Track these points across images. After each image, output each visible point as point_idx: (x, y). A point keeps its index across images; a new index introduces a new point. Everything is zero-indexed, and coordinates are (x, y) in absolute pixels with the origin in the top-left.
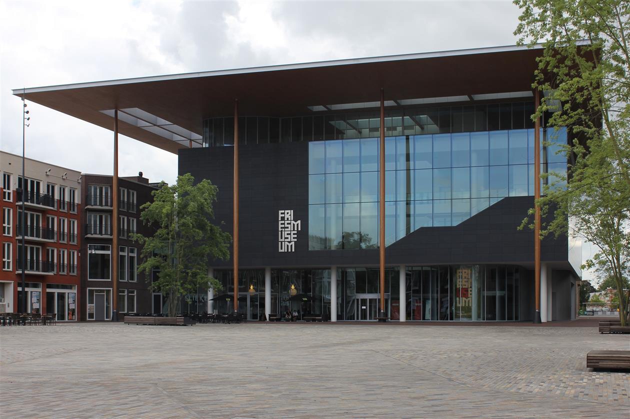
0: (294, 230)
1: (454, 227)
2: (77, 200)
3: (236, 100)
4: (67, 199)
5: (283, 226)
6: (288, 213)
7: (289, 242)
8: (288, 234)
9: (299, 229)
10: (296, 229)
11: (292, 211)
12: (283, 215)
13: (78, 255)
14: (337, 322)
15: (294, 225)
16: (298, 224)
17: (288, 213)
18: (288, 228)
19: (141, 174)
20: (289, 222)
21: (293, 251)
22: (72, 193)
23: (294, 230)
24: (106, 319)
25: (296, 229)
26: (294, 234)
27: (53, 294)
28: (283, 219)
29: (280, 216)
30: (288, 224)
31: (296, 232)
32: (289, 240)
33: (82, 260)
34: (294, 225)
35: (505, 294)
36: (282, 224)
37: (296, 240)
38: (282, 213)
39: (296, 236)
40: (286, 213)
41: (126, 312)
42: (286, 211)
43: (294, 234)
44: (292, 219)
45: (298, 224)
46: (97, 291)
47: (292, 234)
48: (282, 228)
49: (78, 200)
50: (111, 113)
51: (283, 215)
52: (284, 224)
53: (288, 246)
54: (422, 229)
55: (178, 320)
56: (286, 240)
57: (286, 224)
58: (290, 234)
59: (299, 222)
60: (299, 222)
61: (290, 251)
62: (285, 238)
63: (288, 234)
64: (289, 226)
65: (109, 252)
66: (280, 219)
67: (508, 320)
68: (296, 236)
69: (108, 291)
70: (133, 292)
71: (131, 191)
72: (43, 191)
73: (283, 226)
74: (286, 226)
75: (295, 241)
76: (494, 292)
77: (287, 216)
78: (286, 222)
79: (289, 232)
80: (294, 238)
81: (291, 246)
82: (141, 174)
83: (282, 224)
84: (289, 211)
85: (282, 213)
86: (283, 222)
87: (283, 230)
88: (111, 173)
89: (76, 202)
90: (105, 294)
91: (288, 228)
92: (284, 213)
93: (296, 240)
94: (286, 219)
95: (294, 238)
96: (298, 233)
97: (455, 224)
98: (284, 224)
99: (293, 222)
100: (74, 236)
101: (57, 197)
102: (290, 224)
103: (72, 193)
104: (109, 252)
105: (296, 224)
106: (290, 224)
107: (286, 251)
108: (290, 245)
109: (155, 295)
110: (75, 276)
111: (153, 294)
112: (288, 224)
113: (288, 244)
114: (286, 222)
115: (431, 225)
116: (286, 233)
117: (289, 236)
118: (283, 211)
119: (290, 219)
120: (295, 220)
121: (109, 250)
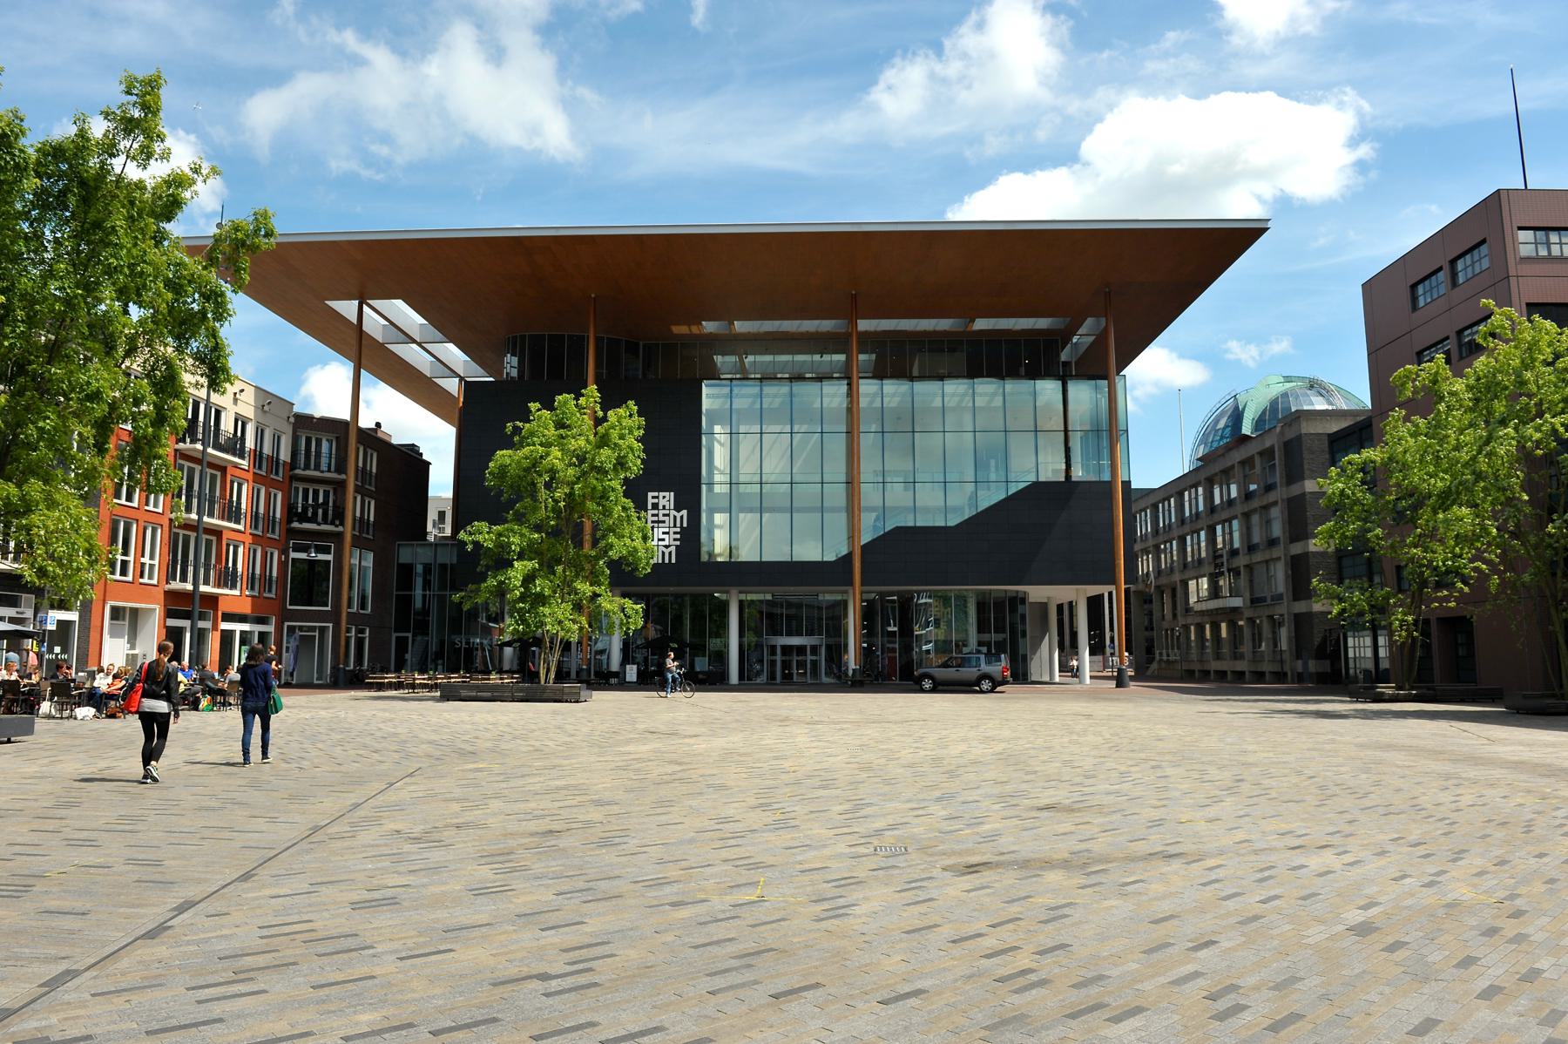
0: (675, 526)
1: (950, 527)
2: (285, 455)
3: (593, 296)
4: (267, 450)
5: (656, 519)
6: (664, 497)
7: (666, 547)
8: (664, 533)
9: (685, 525)
10: (678, 525)
11: (672, 494)
12: (656, 501)
13: (279, 558)
14: (739, 684)
15: (675, 517)
16: (682, 517)
17: (664, 497)
18: (664, 522)
19: (378, 425)
20: (667, 512)
21: (673, 561)
22: (277, 441)
23: (675, 526)
24: (315, 682)
25: (678, 525)
26: (675, 533)
27: (232, 632)
28: (655, 506)
29: (650, 501)
30: (664, 515)
31: (679, 530)
32: (666, 543)
33: (283, 565)
34: (675, 517)
35: (1005, 639)
36: (653, 515)
37: (678, 543)
38: (653, 497)
39: (678, 536)
40: (661, 497)
41: (352, 667)
42: (662, 494)
43: (675, 533)
44: (672, 507)
45: (682, 517)
46: (301, 628)
47: (671, 533)
48: (653, 522)
49: (286, 456)
50: (348, 308)
51: (656, 501)
52: (657, 515)
53: (663, 553)
54: (898, 531)
55: (566, 690)
56: (660, 543)
57: (661, 515)
58: (668, 533)
59: (684, 512)
60: (684, 512)
61: (667, 561)
62: (659, 540)
63: (664, 533)
64: (666, 518)
65: (329, 557)
66: (650, 507)
67: (900, 680)
68: (678, 536)
69: (323, 630)
70: (362, 631)
71: (369, 451)
72: (227, 425)
73: (656, 519)
74: (661, 518)
75: (677, 546)
76: (837, 639)
77: (662, 502)
78: (661, 512)
79: (667, 530)
80: (675, 540)
81: (670, 553)
82: (378, 425)
84: (667, 494)
85: (653, 497)
86: (656, 512)
87: (656, 525)
88: (345, 415)
89: (282, 457)
90: (317, 634)
91: (664, 522)
92: (657, 497)
93: (678, 543)
94: (661, 507)
95: (675, 540)
96: (683, 531)
97: (953, 521)
98: (657, 515)
99: (673, 513)
100: (274, 521)
101: (250, 443)
102: (668, 515)
103: (277, 441)
104: (329, 557)
105: (678, 515)
106: (668, 515)
107: (660, 561)
108: (667, 551)
109: (397, 638)
110: (272, 598)
111: (394, 635)
112: (664, 515)
113: (664, 549)
114: (661, 512)
115: (911, 524)
116: (661, 530)
117: (666, 537)
118: (656, 494)
119: (667, 507)
120: (678, 509)
121: (330, 553)
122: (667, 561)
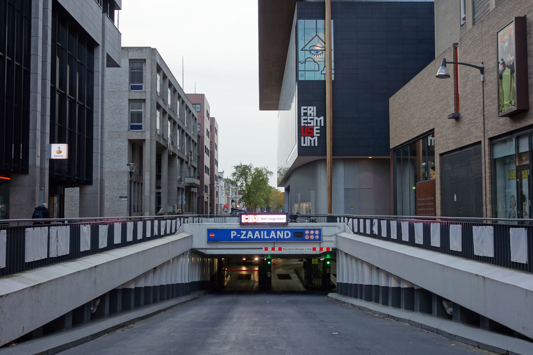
21: (316, 145)
23: (317, 125)
31: (319, 128)
34: (317, 120)
36: (304, 119)
38: (304, 109)
44: (315, 115)
51: (306, 111)
57: (309, 119)
73: (306, 121)
83: (304, 119)
86: (306, 117)
94: (308, 115)
99: (316, 118)
105: (319, 119)
118: (305, 107)
122: (313, 145)
